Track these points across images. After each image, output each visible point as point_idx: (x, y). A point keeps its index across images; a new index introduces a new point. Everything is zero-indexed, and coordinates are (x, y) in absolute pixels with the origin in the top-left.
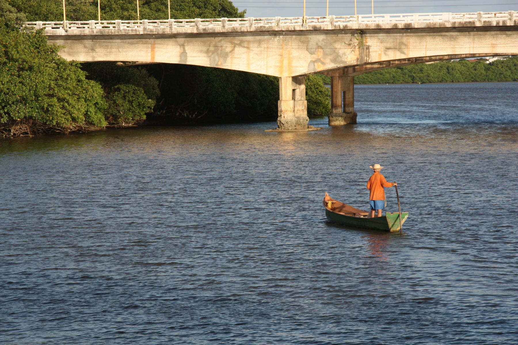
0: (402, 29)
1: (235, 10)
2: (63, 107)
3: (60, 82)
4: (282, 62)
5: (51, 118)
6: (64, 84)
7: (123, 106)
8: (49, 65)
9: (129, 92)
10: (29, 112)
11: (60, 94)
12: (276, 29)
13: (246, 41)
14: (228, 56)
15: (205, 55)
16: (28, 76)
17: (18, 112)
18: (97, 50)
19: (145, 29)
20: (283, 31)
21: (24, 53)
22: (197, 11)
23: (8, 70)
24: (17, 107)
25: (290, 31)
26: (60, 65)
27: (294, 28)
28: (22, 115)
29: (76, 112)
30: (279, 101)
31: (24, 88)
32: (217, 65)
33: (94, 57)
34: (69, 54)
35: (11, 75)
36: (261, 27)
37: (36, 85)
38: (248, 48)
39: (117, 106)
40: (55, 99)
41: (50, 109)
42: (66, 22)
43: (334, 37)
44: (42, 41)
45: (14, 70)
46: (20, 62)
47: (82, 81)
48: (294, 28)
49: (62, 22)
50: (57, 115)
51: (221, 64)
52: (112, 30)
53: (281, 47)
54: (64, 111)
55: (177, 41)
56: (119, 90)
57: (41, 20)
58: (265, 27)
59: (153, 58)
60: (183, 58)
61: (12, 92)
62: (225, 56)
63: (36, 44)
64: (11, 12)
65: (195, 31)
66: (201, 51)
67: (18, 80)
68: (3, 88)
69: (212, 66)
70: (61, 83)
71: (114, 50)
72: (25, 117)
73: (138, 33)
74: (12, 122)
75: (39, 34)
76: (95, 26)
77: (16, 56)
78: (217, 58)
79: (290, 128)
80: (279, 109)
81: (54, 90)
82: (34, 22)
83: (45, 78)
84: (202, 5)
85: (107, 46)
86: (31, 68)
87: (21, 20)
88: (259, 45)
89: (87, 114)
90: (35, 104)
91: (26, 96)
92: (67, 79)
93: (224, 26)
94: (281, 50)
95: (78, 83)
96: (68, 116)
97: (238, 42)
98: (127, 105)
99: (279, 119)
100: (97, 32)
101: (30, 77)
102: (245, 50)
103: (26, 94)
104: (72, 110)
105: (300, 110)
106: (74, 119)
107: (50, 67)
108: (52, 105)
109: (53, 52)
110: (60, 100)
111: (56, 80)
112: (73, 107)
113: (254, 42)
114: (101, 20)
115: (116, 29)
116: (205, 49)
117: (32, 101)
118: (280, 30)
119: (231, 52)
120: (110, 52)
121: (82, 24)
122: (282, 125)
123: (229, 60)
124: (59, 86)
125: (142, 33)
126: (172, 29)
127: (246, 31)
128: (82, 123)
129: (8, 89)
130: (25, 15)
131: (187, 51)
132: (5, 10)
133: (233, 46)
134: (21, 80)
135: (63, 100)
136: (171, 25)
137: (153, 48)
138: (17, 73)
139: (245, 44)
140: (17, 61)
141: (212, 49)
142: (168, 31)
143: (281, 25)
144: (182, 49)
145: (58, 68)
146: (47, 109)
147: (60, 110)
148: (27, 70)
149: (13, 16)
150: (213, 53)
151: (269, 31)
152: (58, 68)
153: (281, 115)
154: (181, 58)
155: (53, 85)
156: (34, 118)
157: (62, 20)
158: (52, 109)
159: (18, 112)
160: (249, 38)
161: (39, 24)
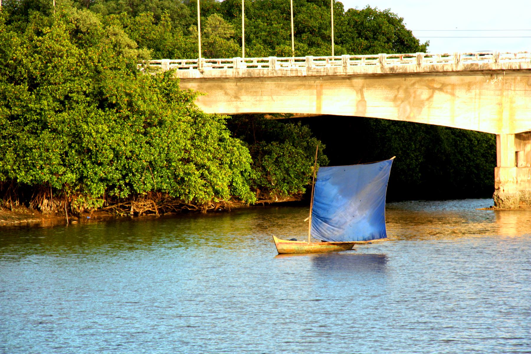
0: (462, 71)
1: (415, 41)
2: (202, 176)
3: (197, 142)
4: (501, 113)
5: (187, 191)
6: (203, 145)
7: (275, 174)
8: (183, 119)
9: (284, 155)
10: (157, 183)
11: (198, 159)
12: (494, 68)
13: (450, 84)
14: (423, 105)
15: (392, 104)
16: (158, 135)
17: (144, 183)
18: (244, 98)
19: (309, 69)
20: (503, 70)
21: (151, 103)
22: (365, 43)
23: (131, 126)
24: (142, 176)
25: (514, 70)
26: (197, 119)
27: (520, 66)
28: (149, 187)
29: (220, 183)
30: (496, 169)
31: (153, 150)
32: (408, 117)
33: (237, 107)
34: (205, 103)
35: (135, 132)
36: (472, 64)
37: (168, 146)
38: (453, 94)
39: (266, 175)
40: (192, 166)
41: (186, 179)
42: (201, 60)
43: (368, 81)
44: (174, 85)
45: (139, 125)
46: (147, 115)
47: (225, 139)
48: (520, 66)
49: (195, 60)
50: (195, 187)
51: (414, 117)
52: (259, 71)
53: (499, 92)
54: (203, 182)
55: (352, 86)
56: (269, 153)
57: (164, 58)
58: (477, 65)
59: (319, 108)
60: (361, 108)
61: (137, 155)
62: (420, 104)
63: (166, 89)
64: (130, 47)
65: (379, 71)
66: (386, 99)
67: (145, 139)
68: (125, 150)
69: (402, 120)
70: (199, 143)
71: (265, 98)
72: (152, 190)
73: (299, 74)
74: (134, 195)
75: (168, 76)
76: (240, 65)
77: (143, 107)
78: (408, 108)
79: (512, 207)
80: (496, 180)
81: (190, 153)
82: (158, 61)
83: (180, 138)
84: (370, 34)
85: (255, 92)
86: (161, 123)
87: (143, 58)
88: (469, 90)
89: (231, 185)
90: (166, 172)
91: (155, 161)
92: (206, 137)
93: (419, 64)
94: (499, 97)
95: (220, 143)
96: (210, 189)
97: (438, 86)
98: (280, 174)
99: (495, 193)
100: (243, 74)
101: (160, 135)
102: (449, 96)
103: (154, 158)
104: (215, 180)
105: (524, 181)
106: (217, 193)
107: (183, 122)
108: (189, 174)
109: (188, 101)
110: (199, 167)
111: (193, 140)
112: (216, 176)
113: (462, 85)
114: (335, 55)
115: (270, 68)
116: (391, 94)
117: (162, 168)
118: (499, 68)
119: (428, 99)
120: (260, 101)
121: (222, 63)
122: (500, 201)
123: (425, 110)
124: (196, 147)
125: (305, 74)
126: (346, 69)
127: (451, 70)
128: (227, 199)
129: (131, 152)
130: (149, 52)
131: (366, 99)
132: (122, 46)
133: (431, 90)
134: (148, 139)
135: (203, 166)
136: (345, 63)
137: (319, 95)
138: (143, 131)
139: (449, 89)
140: (143, 113)
141: (401, 94)
142: (340, 71)
143: (500, 61)
144: (360, 95)
145: (195, 123)
146: (182, 179)
147: (199, 180)
148: (155, 126)
149: (134, 53)
150: (403, 101)
151: (482, 71)
152: (195, 123)
153: (499, 188)
154: (358, 109)
155: (189, 146)
156: (163, 191)
157: (197, 57)
158: (189, 179)
159: (144, 183)
160: (454, 79)
161: (166, 64)
